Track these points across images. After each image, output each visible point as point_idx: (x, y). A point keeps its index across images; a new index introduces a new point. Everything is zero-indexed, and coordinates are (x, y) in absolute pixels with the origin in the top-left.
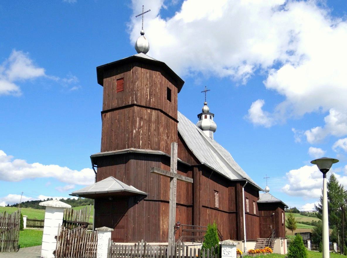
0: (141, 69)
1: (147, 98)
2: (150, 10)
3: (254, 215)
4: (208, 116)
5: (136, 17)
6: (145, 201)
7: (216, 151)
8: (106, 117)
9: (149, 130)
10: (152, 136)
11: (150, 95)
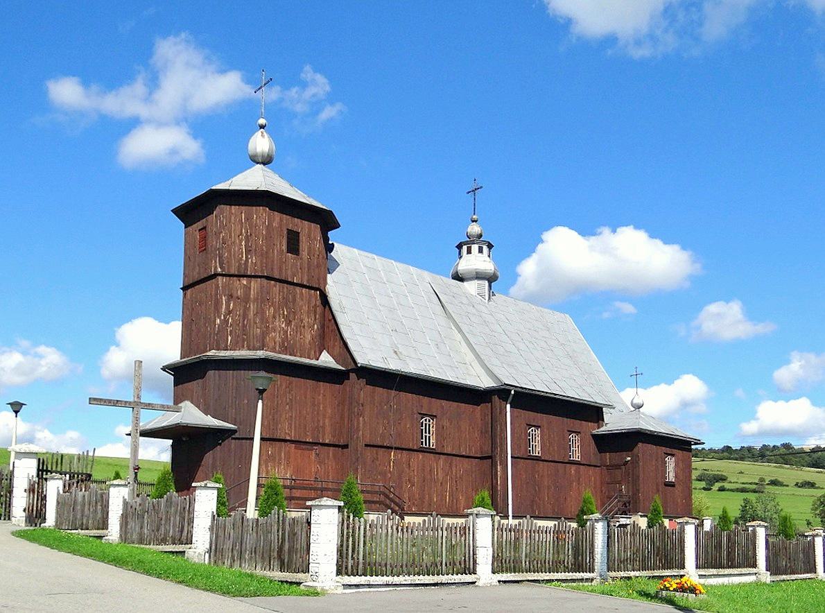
0: (230, 209)
1: (241, 259)
2: (271, 79)
3: (537, 459)
4: (475, 248)
5: (271, 79)
6: (234, 441)
7: (460, 331)
8: (304, 252)
9: (245, 316)
10: (250, 327)
11: (248, 252)
